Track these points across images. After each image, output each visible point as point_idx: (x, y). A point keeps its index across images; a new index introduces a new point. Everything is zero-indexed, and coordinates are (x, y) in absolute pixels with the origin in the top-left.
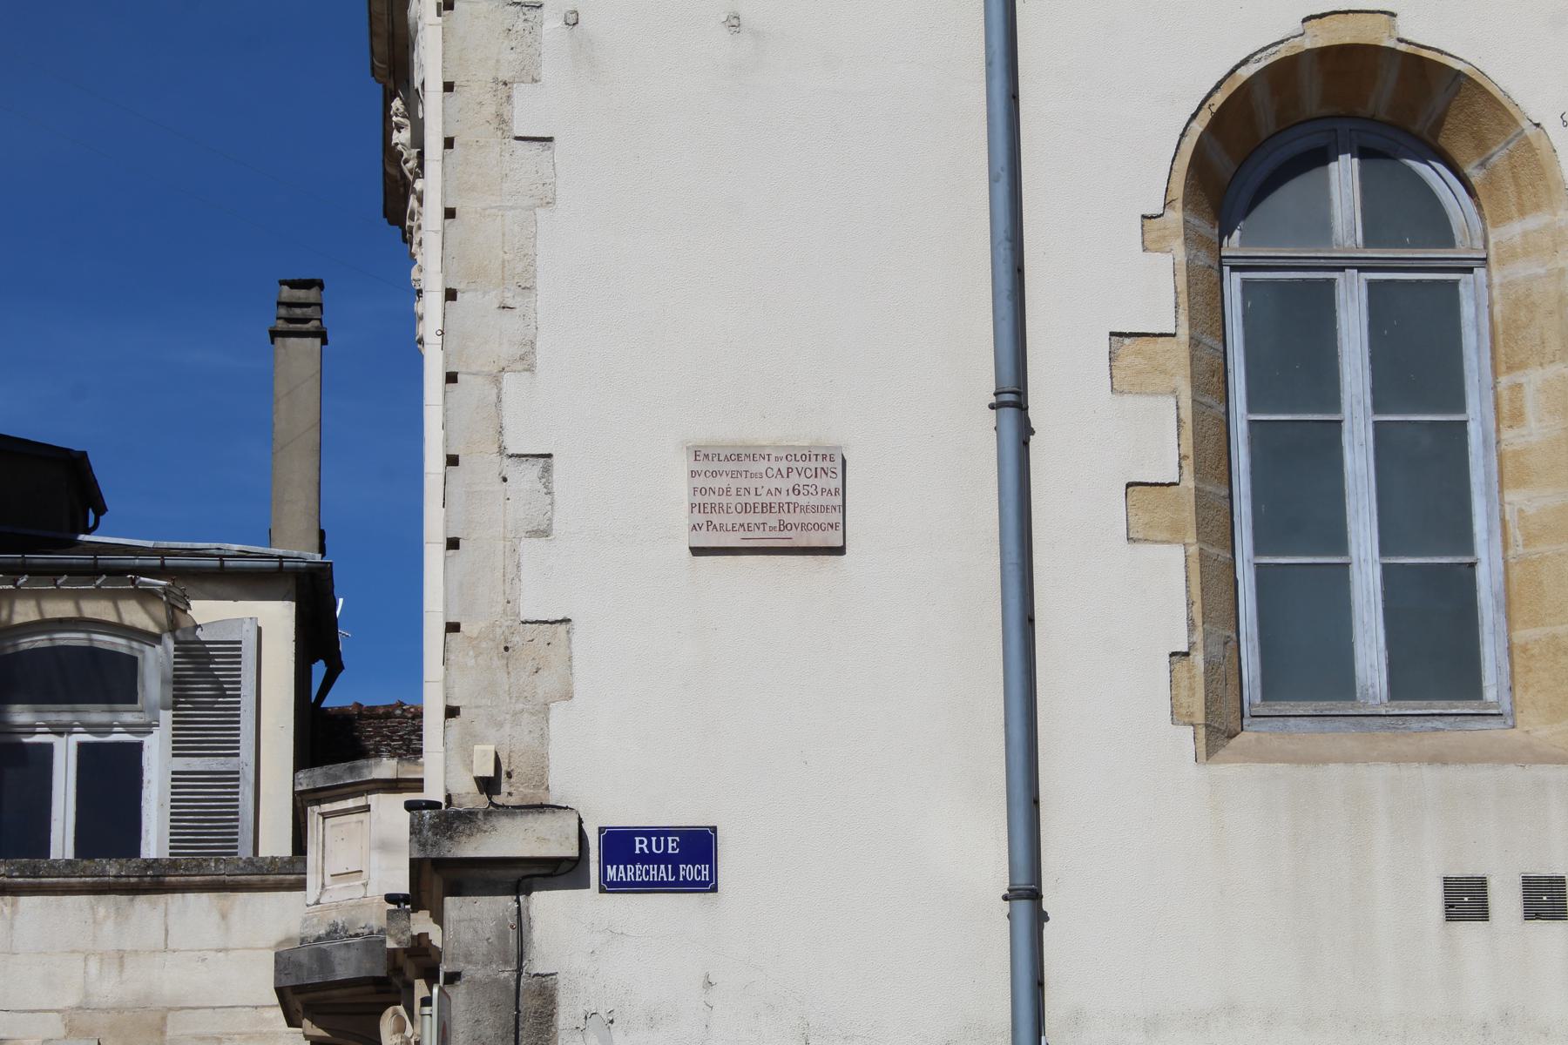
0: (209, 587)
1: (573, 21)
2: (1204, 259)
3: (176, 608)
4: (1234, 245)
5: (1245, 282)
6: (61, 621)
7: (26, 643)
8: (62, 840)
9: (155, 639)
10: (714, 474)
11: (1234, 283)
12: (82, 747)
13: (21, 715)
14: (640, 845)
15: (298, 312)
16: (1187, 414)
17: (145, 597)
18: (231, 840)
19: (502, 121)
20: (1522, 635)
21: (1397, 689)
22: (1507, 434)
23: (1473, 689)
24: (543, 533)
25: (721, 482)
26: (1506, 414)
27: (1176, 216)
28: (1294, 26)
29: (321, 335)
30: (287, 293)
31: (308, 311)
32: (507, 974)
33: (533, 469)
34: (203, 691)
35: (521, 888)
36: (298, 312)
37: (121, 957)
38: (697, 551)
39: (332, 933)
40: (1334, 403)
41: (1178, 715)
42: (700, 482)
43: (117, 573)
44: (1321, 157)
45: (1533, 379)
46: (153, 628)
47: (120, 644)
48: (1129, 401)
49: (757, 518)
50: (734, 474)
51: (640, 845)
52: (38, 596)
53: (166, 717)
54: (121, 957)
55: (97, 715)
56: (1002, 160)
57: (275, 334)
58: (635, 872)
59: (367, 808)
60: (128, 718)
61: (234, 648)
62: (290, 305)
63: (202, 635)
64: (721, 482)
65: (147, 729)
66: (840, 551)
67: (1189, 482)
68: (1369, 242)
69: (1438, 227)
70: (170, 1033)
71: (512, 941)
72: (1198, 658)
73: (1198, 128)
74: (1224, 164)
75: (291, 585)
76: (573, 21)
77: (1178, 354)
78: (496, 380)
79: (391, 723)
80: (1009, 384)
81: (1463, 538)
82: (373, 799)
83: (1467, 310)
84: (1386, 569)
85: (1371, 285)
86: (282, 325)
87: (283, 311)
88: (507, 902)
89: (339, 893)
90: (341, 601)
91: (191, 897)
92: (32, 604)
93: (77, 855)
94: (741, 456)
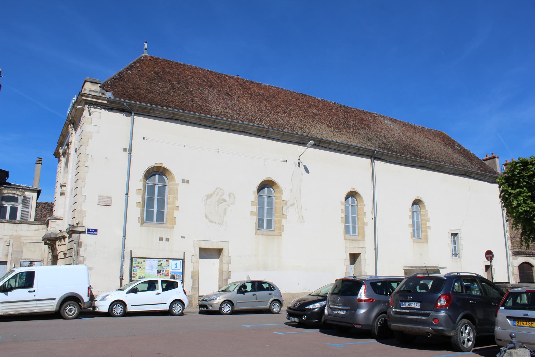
0: (27, 191)
1: (91, 156)
2: (145, 183)
3: (24, 192)
4: (147, 182)
5: (148, 185)
6: (10, 193)
7: (5, 195)
8: (8, 217)
9: (21, 196)
10: (100, 198)
11: (147, 185)
12: (11, 207)
13: (4, 203)
14: (91, 230)
15: (39, 161)
16: (142, 196)
17: (20, 191)
18: (27, 218)
19: (84, 165)
20: (168, 217)
21: (157, 221)
22: (168, 200)
23: (163, 221)
24: (84, 202)
25: (101, 199)
26: (168, 198)
27: (143, 179)
28: (154, 164)
29: (41, 164)
30: (38, 159)
31: (40, 161)
32: (78, 241)
33: (84, 196)
34: (26, 202)
35: (80, 233)
36: (39, 161)
37: (16, 230)
38: (98, 205)
39: (51, 233)
40: (154, 196)
41: (139, 222)
42: (99, 199)
43: (17, 188)
44: (155, 175)
45: (171, 196)
46: (21, 195)
47: (16, 196)
48: (137, 195)
49: (104, 202)
50: (102, 198)
51: (91, 230)
52: (7, 190)
53: (21, 204)
54: (16, 230)
55: (13, 203)
56: (128, 173)
57: (36, 163)
58: (90, 233)
59: (56, 221)
60: (17, 204)
61: (30, 198)
62: (38, 160)
63: (26, 196)
64: (101, 199)
65: (18, 205)
66: (111, 206)
67: (141, 202)
68: (159, 182)
69: (164, 182)
70: (21, 239)
71: (78, 238)
72: (141, 217)
73: (146, 172)
74: (147, 175)
75: (37, 191)
76: (91, 156)
77: (142, 191)
78: (81, 188)
79: (40, 204)
80: (127, 193)
81: (164, 208)
82: (57, 220)
83: (166, 189)
84: (157, 211)
85: (158, 186)
86: (37, 162)
87: (37, 161)
88: (78, 234)
89: (52, 229)
90: (237, 308)
91: (25, 225)
92: (6, 191)
93: (9, 219)
94: (103, 197)
